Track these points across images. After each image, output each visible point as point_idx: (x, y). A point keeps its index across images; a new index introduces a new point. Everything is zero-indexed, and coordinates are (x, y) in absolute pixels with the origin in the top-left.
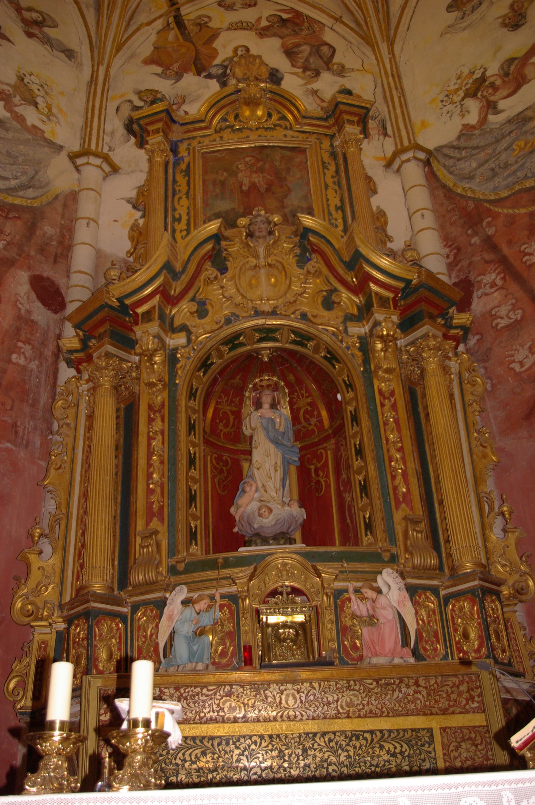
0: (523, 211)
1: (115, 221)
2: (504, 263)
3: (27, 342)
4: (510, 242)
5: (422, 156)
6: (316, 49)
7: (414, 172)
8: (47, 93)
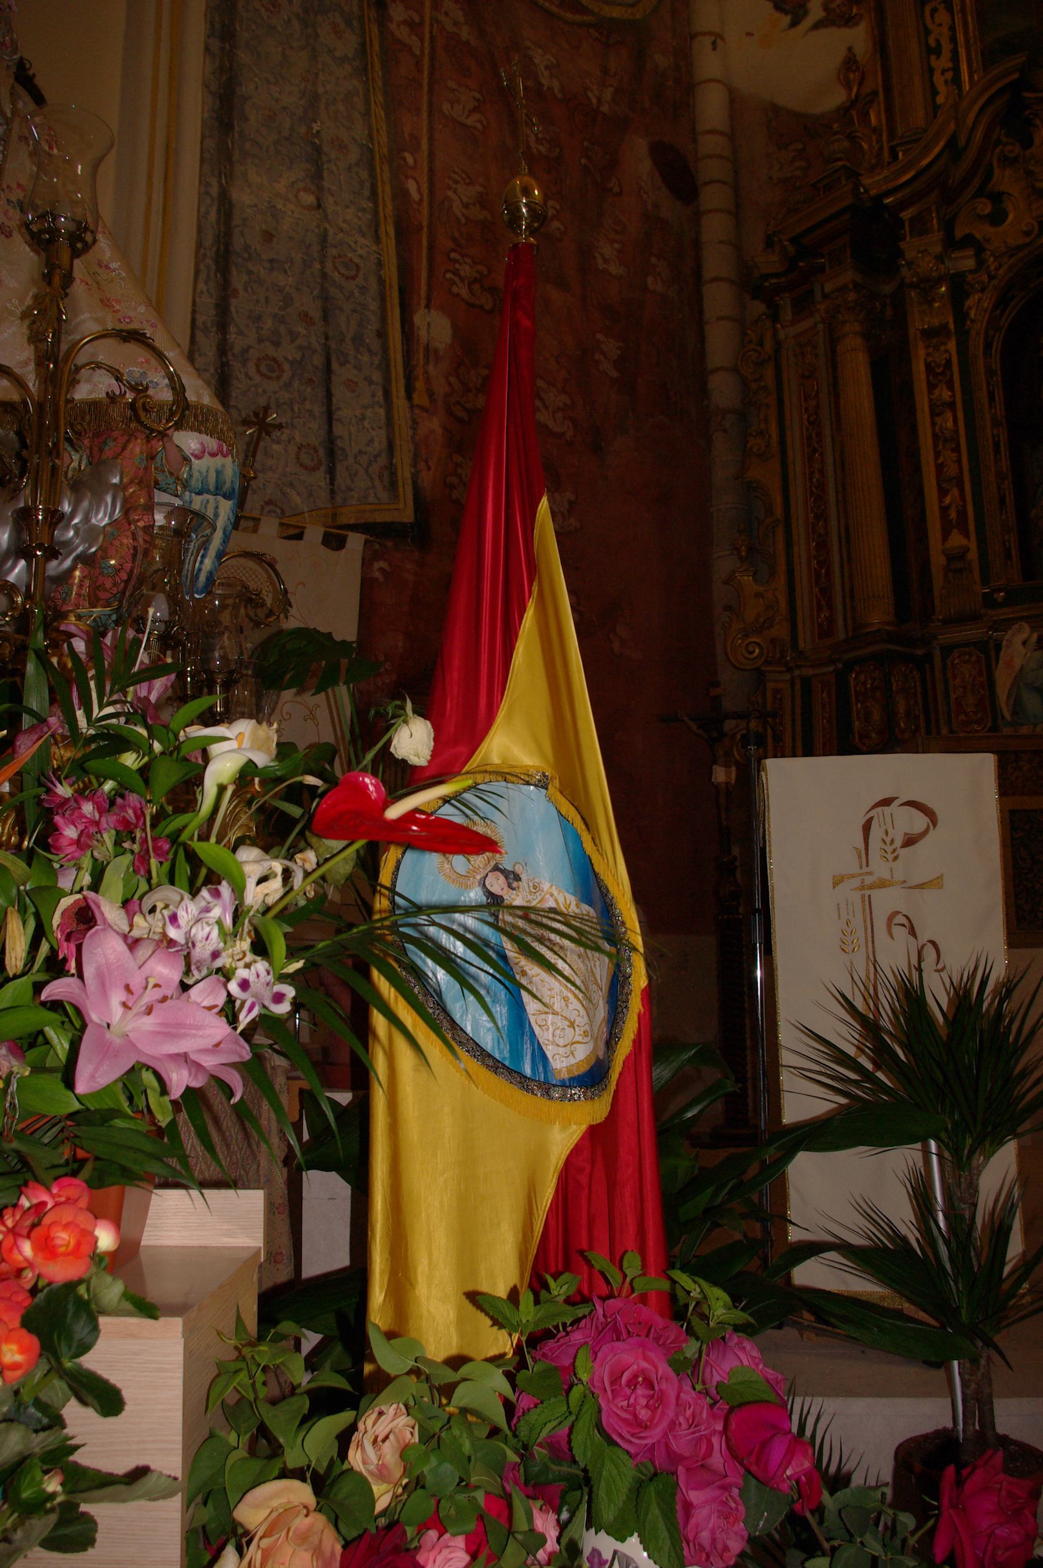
1: (748, 34)
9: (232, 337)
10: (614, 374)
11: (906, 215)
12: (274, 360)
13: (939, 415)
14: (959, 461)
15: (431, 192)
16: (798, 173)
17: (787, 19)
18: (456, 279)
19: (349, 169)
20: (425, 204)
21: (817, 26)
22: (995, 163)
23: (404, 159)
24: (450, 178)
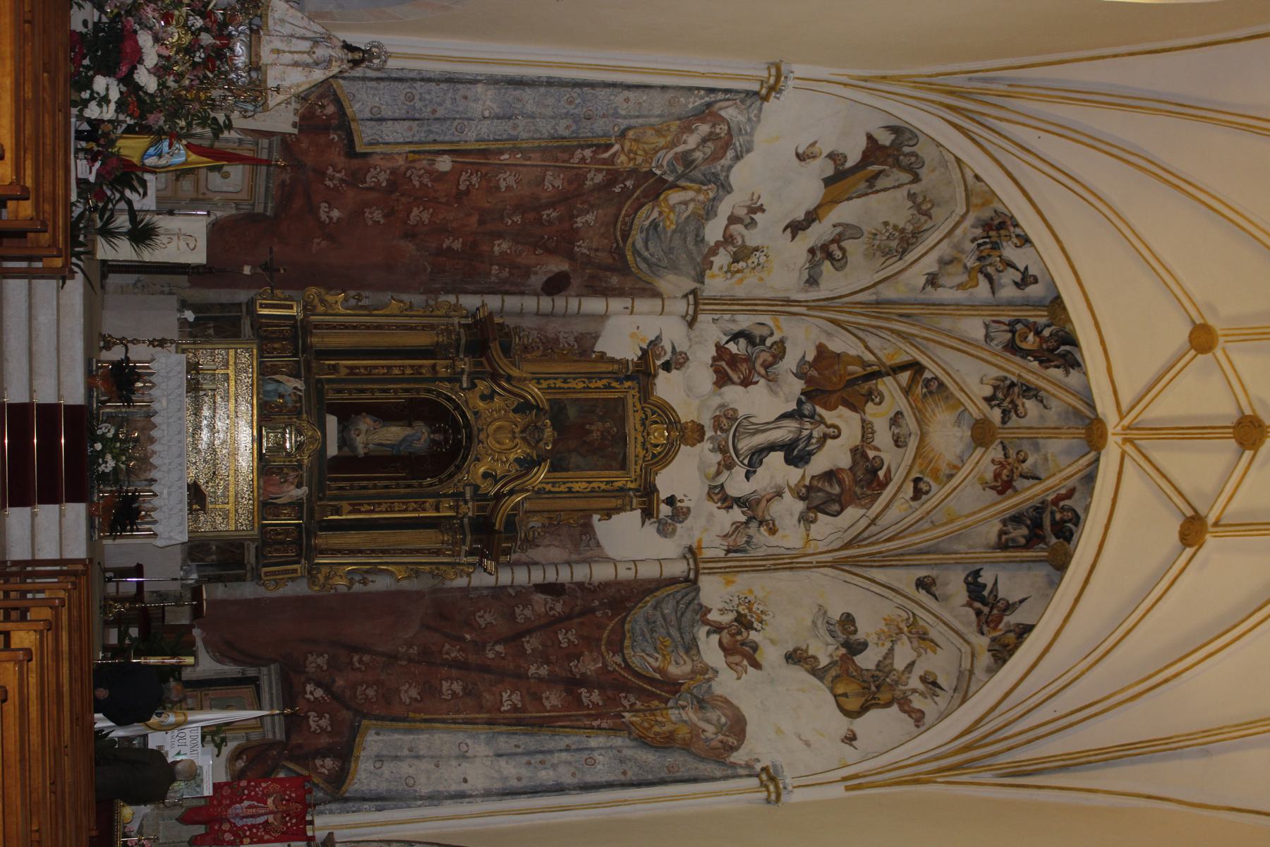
0: (605, 635)
2: (569, 617)
3: (511, 274)
4: (582, 624)
5: (692, 576)
6: (831, 499)
7: (678, 569)
8: (754, 269)
10: (445, 246)
11: (483, 359)
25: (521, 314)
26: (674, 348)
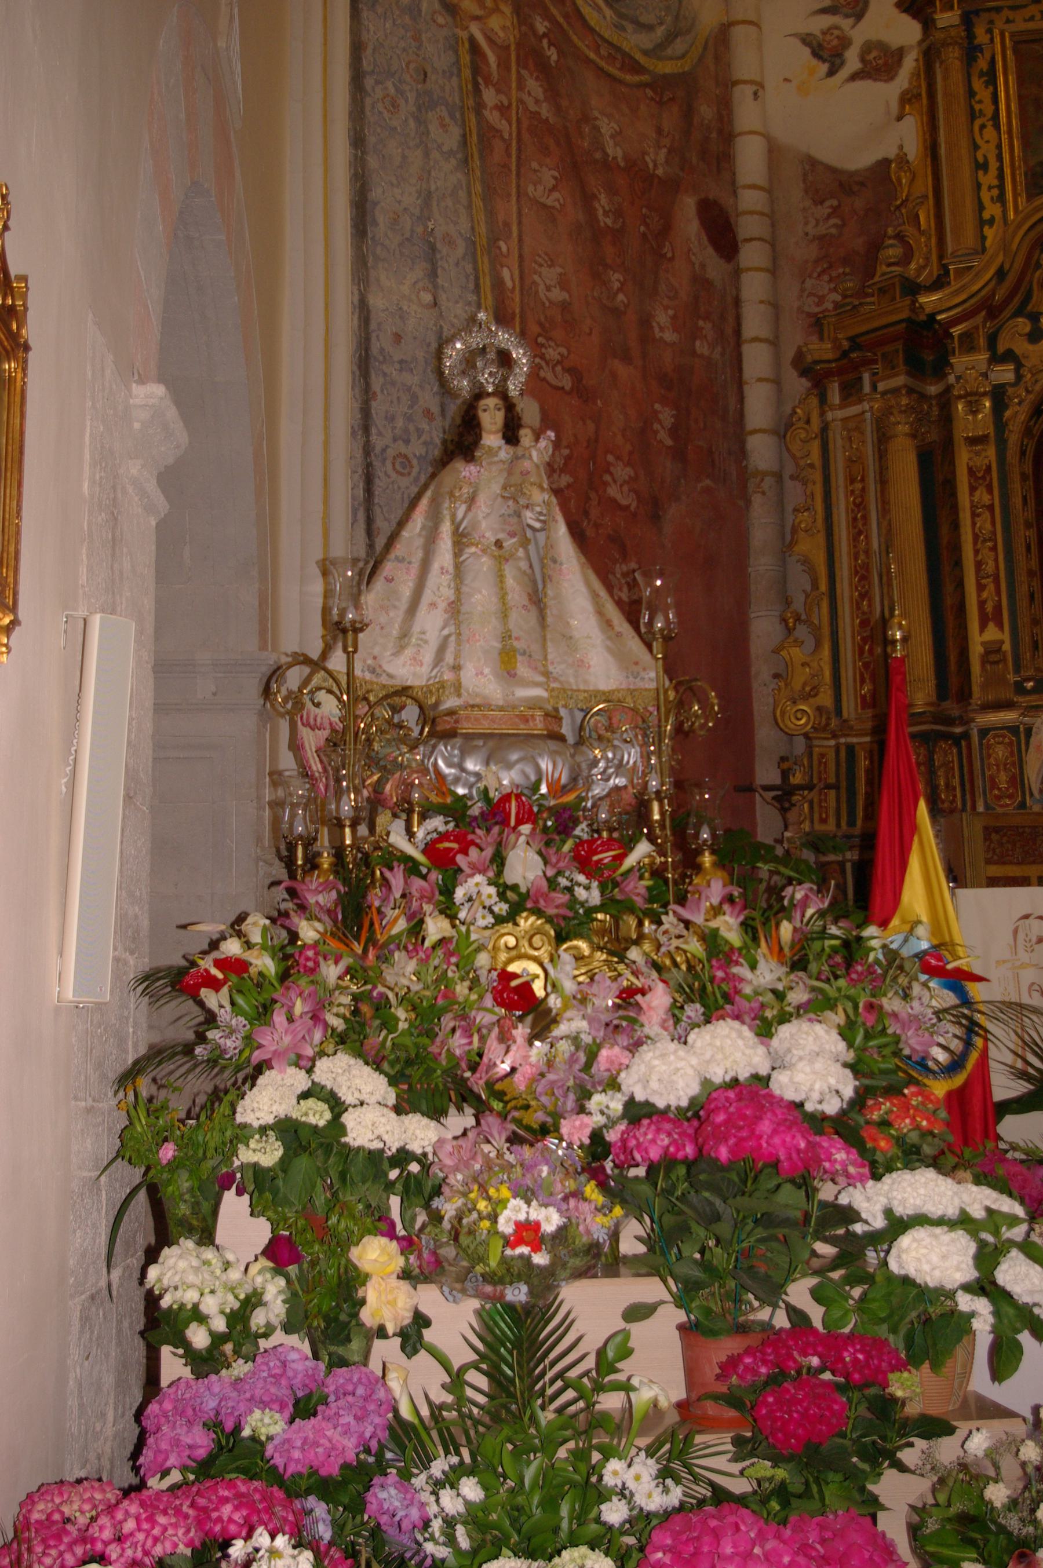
1: (786, 80)
3: (707, 318)
9: (374, 438)
10: (669, 442)
11: (956, 331)
12: (405, 456)
13: (979, 515)
14: (996, 560)
15: (521, 278)
16: (833, 231)
17: (824, 68)
18: (543, 364)
19: (457, 264)
20: (517, 289)
21: (854, 77)
22: (1035, 287)
23: (499, 248)
24: (536, 262)
25: (775, 306)
26: (824, 11)
